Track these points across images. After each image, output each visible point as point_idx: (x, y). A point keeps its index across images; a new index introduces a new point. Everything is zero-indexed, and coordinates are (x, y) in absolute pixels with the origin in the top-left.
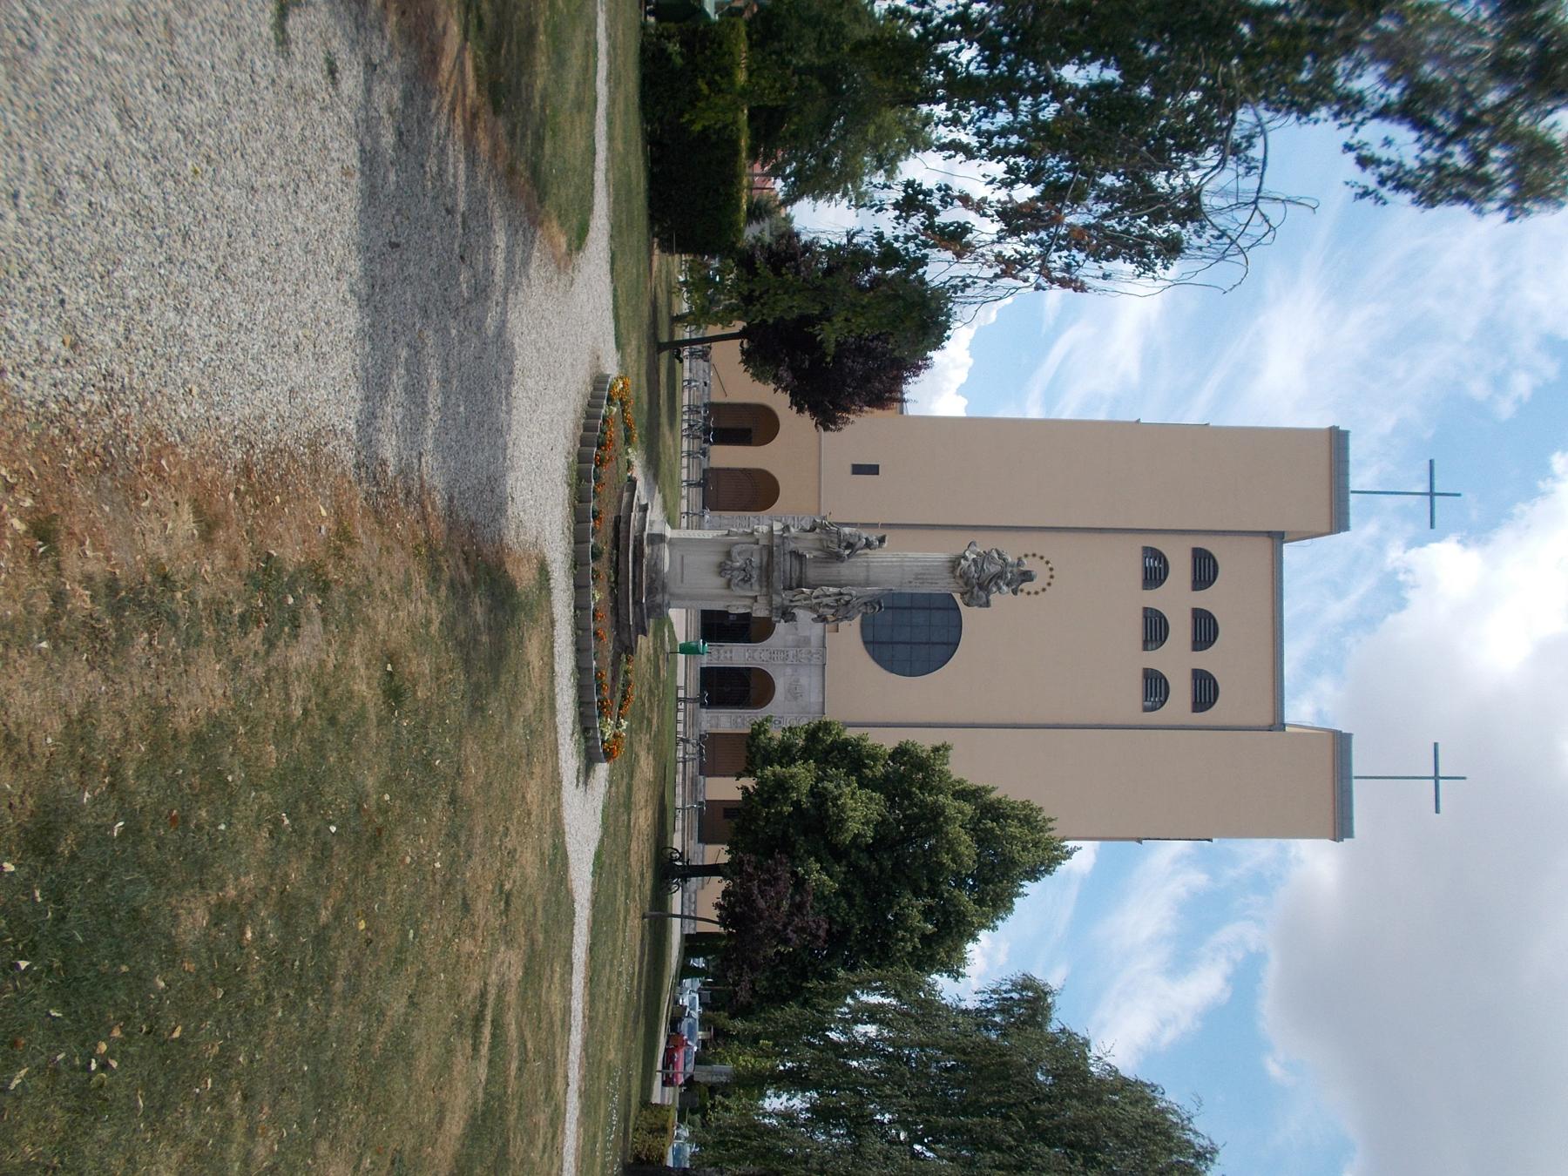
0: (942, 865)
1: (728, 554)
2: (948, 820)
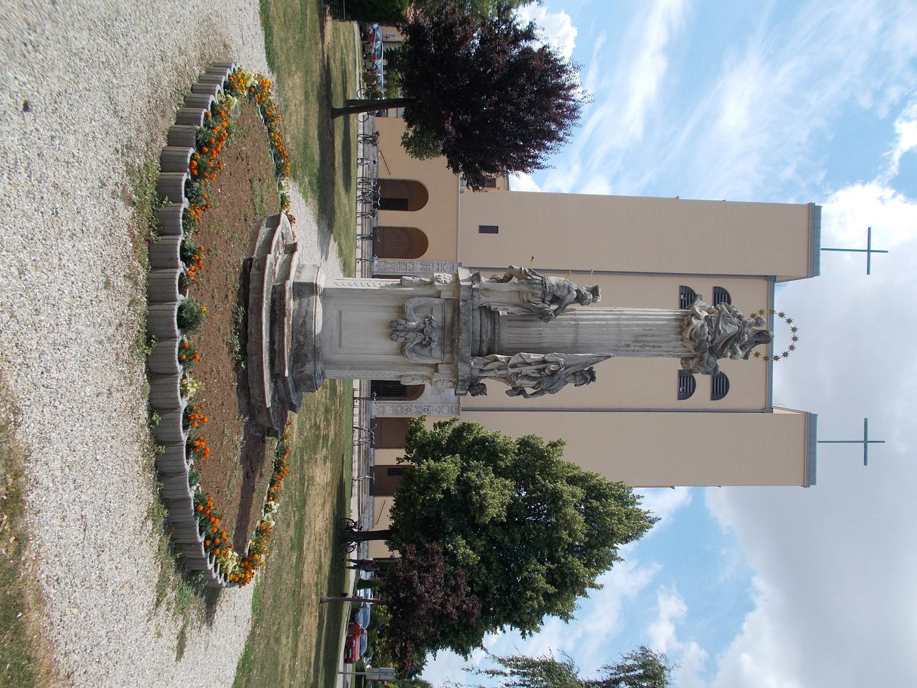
0: (560, 538)
1: (401, 310)
2: (565, 504)
